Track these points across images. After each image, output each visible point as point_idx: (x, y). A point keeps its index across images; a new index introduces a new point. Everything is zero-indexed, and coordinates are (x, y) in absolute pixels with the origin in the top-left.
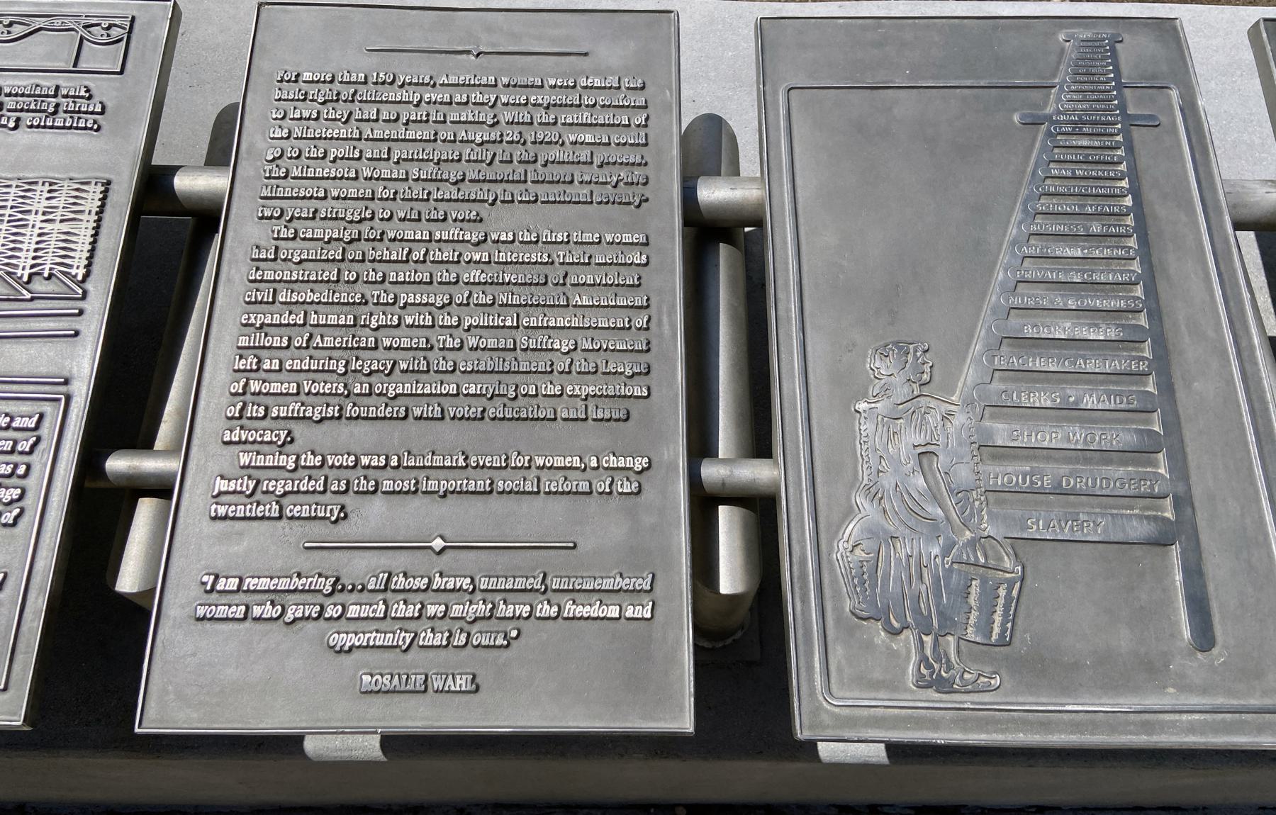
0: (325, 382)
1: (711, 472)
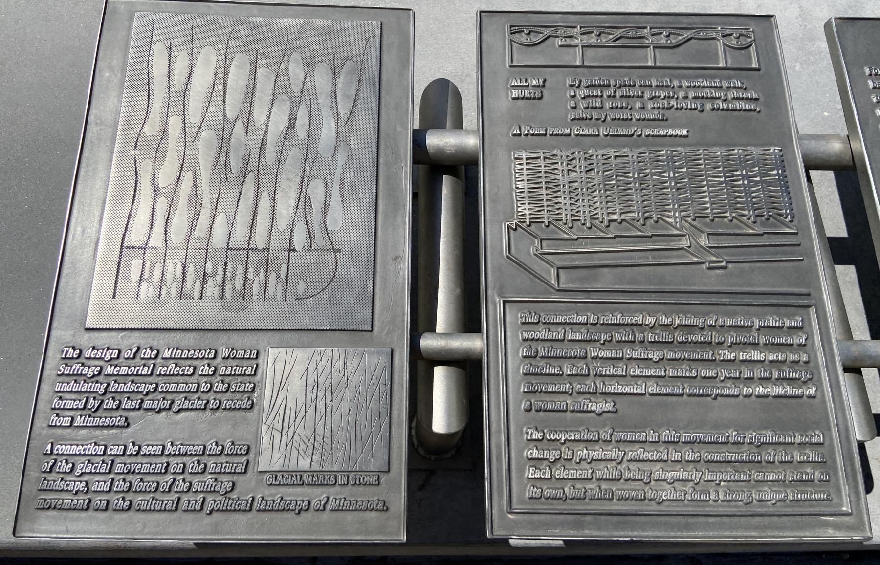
1: (427, 342)
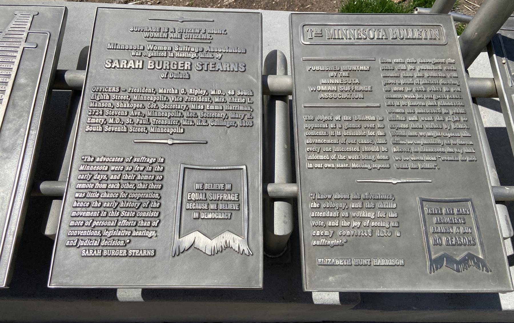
0: (132, 202)
1: (270, 188)
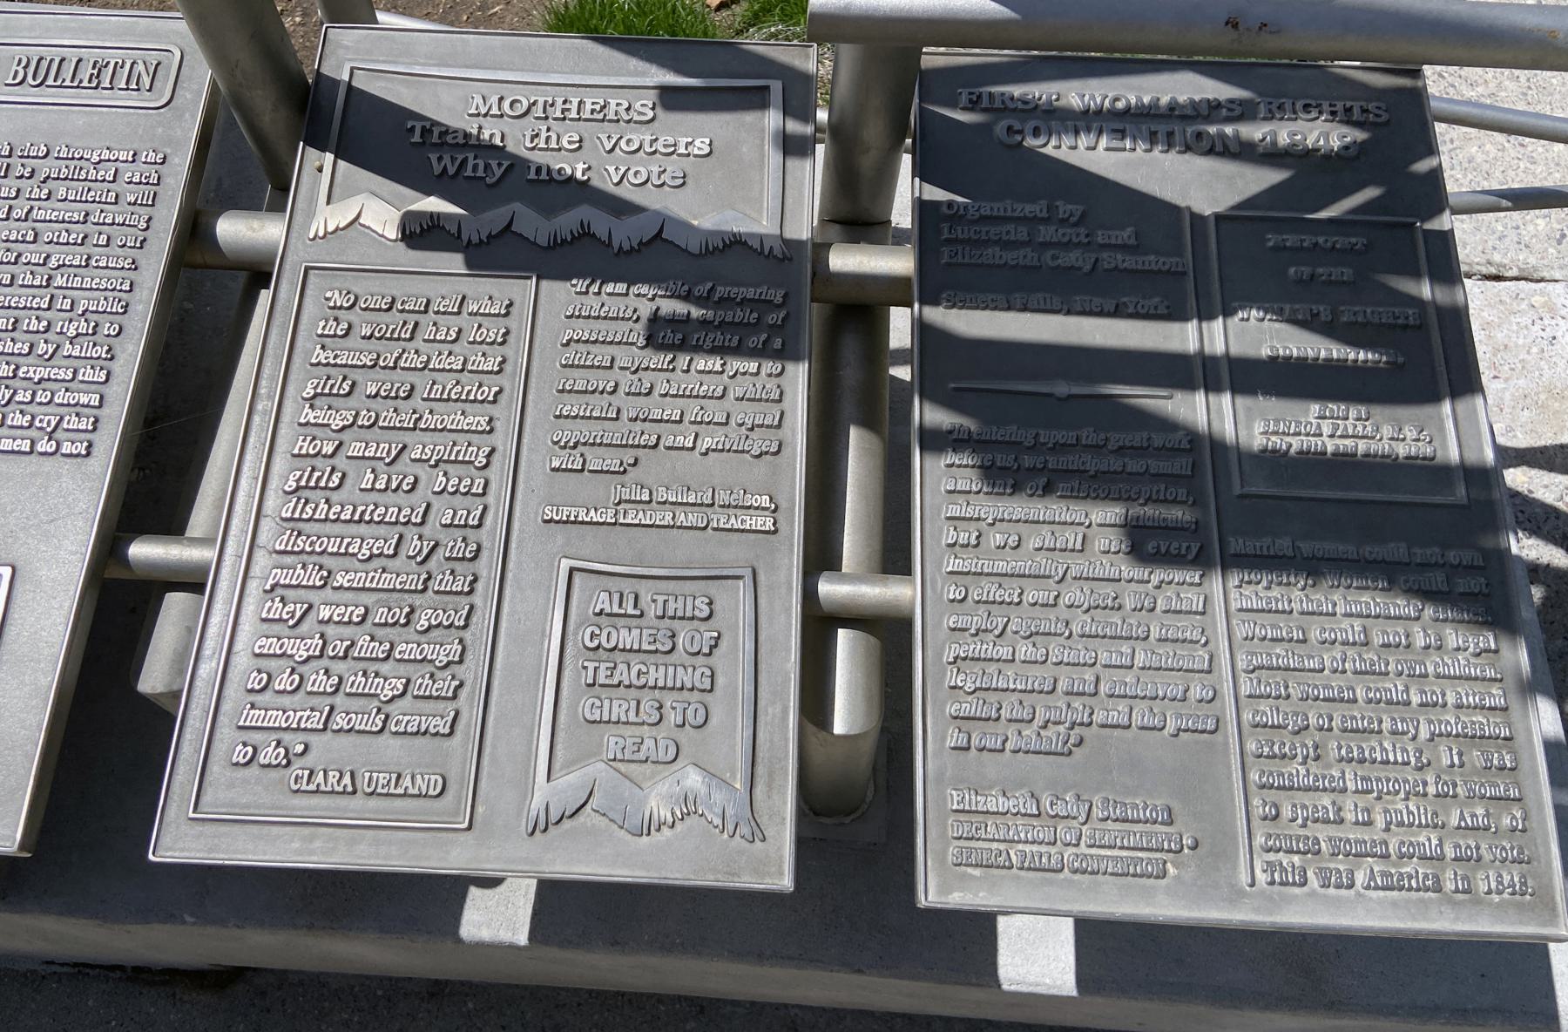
1: (830, 589)
